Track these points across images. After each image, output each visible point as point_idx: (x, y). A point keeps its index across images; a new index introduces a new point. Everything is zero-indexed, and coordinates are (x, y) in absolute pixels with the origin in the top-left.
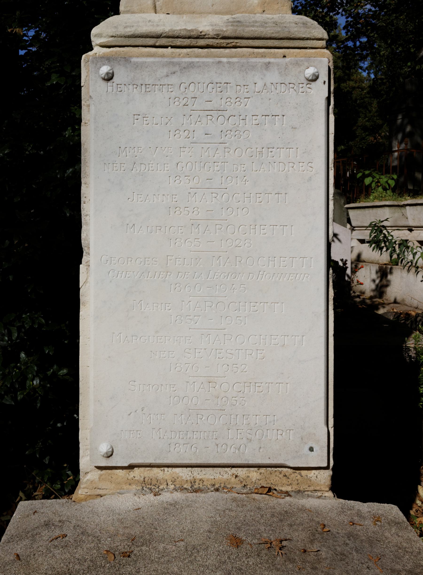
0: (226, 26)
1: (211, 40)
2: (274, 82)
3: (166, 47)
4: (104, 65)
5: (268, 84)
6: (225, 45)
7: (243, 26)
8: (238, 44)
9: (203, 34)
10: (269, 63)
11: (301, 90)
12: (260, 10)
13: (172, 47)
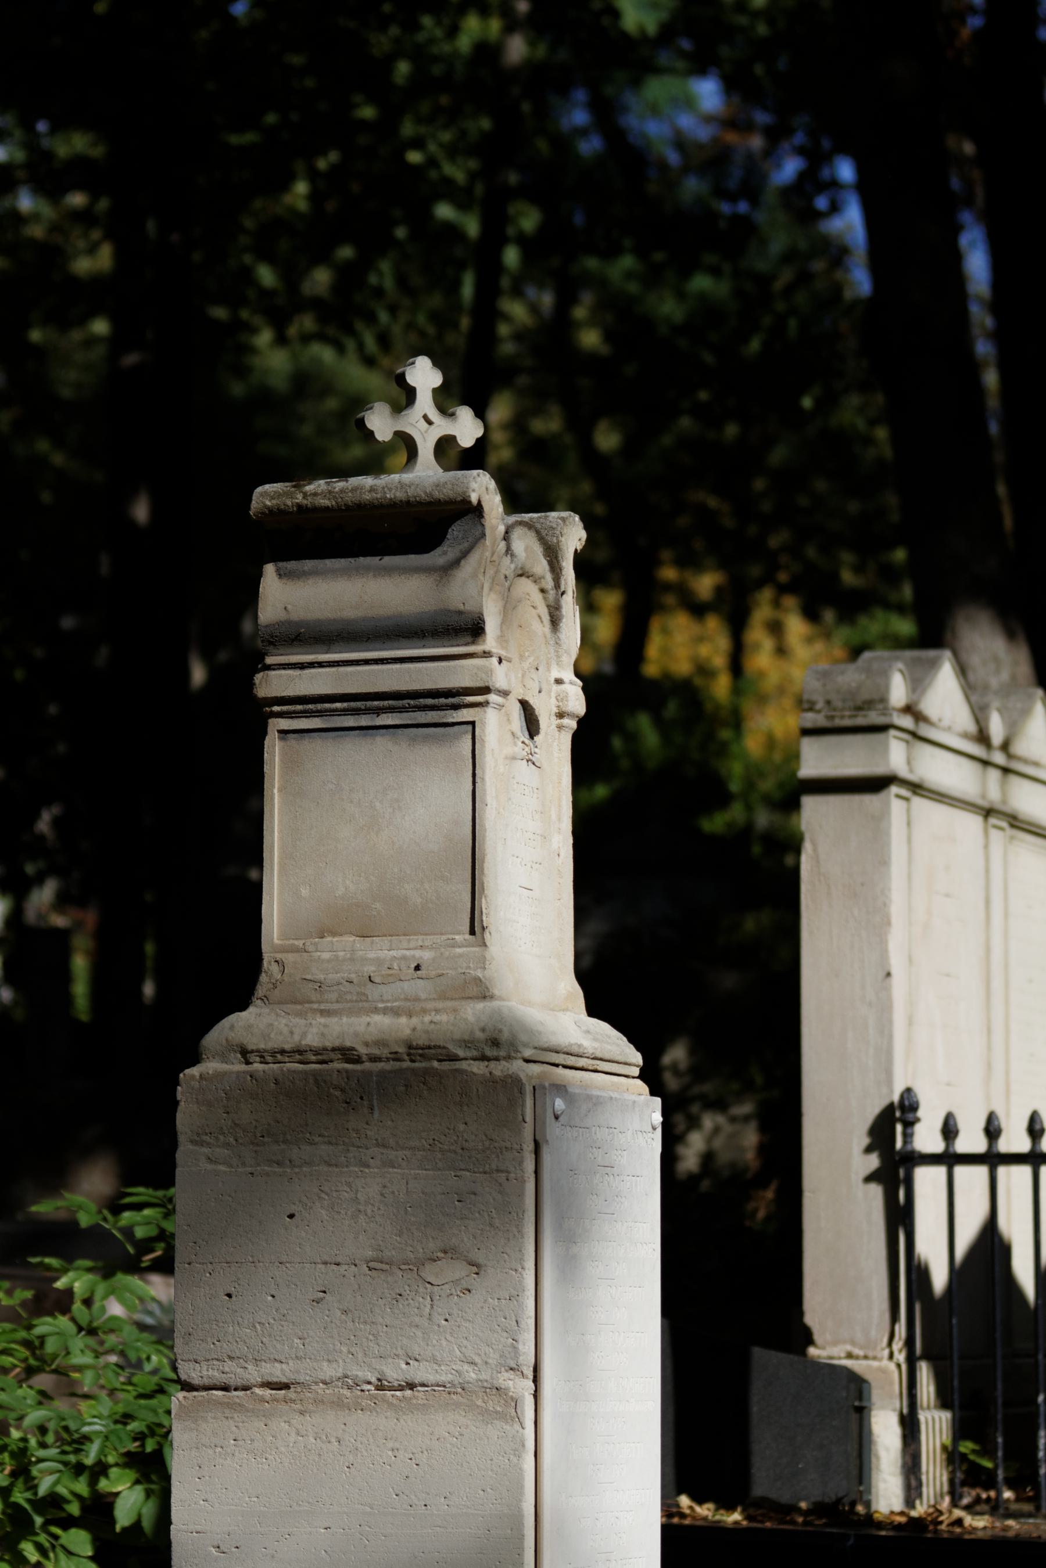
3: (557, 1065)
8: (599, 1069)
13: (565, 1067)
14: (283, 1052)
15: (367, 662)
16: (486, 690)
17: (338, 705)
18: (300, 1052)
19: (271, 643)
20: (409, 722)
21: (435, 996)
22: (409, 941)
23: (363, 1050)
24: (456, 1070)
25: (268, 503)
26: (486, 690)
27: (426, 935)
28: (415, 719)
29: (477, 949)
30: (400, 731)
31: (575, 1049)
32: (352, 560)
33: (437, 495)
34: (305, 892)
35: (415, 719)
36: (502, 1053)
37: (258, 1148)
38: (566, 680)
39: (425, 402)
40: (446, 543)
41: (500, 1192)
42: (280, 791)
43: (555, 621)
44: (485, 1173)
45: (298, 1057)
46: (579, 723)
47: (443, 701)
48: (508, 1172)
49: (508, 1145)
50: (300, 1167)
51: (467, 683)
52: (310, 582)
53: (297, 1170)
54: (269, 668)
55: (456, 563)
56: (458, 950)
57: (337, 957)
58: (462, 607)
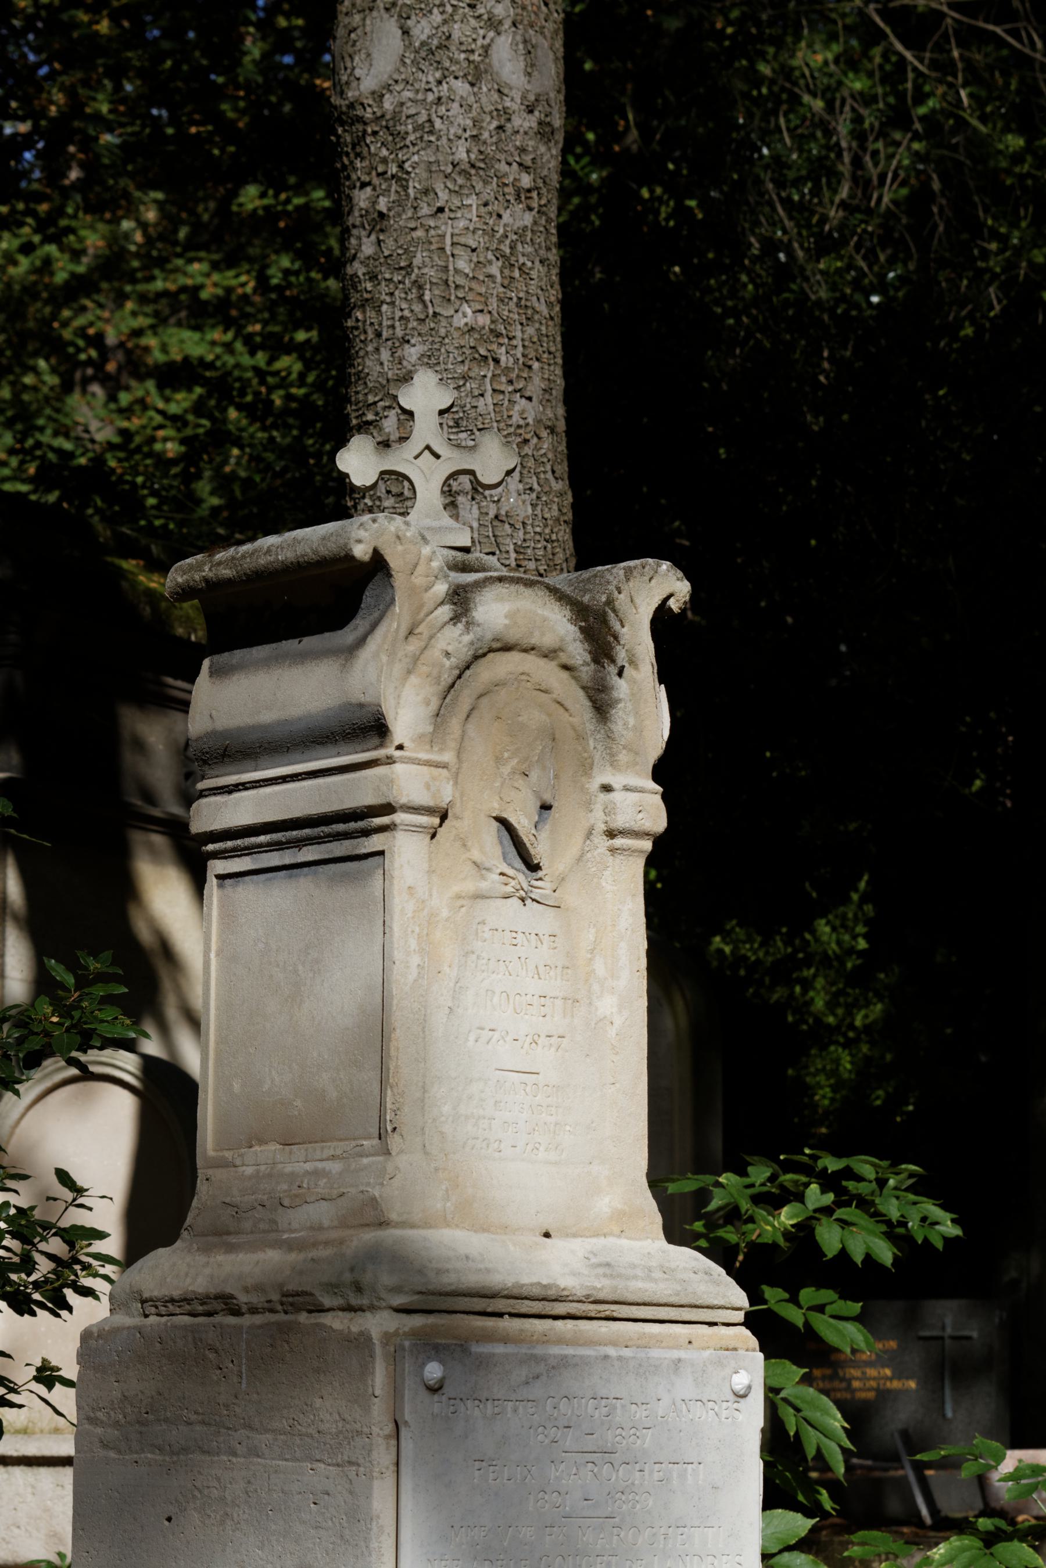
0: (597, 1276)
1: (575, 1305)
2: (687, 1398)
3: (500, 1315)
4: (430, 1359)
5: (679, 1402)
6: (593, 1315)
7: (620, 1276)
8: (615, 1314)
9: (565, 1293)
10: (679, 1360)
11: (725, 1413)
12: (616, 1230)
13: (512, 1315)
14: (172, 1301)
15: (284, 779)
16: (388, 809)
17: (262, 839)
18: (187, 1300)
19: (205, 762)
20: (327, 856)
21: (336, 1223)
22: (322, 1148)
23: (243, 1298)
24: (317, 1325)
25: (180, 580)
26: (388, 809)
27: (341, 1140)
28: (332, 851)
29: (381, 1158)
30: (320, 869)
31: (552, 1293)
32: (274, 645)
33: (324, 551)
34: (236, 1087)
35: (332, 851)
36: (365, 1302)
37: (143, 1429)
38: (615, 786)
39: (426, 429)
40: (361, 613)
41: (351, 1493)
42: (217, 955)
43: (601, 703)
44: (338, 1465)
45: (188, 1307)
46: (654, 843)
47: (353, 825)
48: (359, 1465)
49: (358, 1426)
50: (178, 1454)
51: (369, 799)
52: (235, 678)
53: (175, 1458)
54: (202, 794)
55: (361, 641)
56: (365, 1161)
57: (258, 1171)
58: (363, 699)
